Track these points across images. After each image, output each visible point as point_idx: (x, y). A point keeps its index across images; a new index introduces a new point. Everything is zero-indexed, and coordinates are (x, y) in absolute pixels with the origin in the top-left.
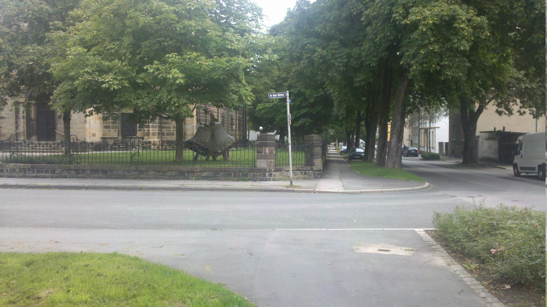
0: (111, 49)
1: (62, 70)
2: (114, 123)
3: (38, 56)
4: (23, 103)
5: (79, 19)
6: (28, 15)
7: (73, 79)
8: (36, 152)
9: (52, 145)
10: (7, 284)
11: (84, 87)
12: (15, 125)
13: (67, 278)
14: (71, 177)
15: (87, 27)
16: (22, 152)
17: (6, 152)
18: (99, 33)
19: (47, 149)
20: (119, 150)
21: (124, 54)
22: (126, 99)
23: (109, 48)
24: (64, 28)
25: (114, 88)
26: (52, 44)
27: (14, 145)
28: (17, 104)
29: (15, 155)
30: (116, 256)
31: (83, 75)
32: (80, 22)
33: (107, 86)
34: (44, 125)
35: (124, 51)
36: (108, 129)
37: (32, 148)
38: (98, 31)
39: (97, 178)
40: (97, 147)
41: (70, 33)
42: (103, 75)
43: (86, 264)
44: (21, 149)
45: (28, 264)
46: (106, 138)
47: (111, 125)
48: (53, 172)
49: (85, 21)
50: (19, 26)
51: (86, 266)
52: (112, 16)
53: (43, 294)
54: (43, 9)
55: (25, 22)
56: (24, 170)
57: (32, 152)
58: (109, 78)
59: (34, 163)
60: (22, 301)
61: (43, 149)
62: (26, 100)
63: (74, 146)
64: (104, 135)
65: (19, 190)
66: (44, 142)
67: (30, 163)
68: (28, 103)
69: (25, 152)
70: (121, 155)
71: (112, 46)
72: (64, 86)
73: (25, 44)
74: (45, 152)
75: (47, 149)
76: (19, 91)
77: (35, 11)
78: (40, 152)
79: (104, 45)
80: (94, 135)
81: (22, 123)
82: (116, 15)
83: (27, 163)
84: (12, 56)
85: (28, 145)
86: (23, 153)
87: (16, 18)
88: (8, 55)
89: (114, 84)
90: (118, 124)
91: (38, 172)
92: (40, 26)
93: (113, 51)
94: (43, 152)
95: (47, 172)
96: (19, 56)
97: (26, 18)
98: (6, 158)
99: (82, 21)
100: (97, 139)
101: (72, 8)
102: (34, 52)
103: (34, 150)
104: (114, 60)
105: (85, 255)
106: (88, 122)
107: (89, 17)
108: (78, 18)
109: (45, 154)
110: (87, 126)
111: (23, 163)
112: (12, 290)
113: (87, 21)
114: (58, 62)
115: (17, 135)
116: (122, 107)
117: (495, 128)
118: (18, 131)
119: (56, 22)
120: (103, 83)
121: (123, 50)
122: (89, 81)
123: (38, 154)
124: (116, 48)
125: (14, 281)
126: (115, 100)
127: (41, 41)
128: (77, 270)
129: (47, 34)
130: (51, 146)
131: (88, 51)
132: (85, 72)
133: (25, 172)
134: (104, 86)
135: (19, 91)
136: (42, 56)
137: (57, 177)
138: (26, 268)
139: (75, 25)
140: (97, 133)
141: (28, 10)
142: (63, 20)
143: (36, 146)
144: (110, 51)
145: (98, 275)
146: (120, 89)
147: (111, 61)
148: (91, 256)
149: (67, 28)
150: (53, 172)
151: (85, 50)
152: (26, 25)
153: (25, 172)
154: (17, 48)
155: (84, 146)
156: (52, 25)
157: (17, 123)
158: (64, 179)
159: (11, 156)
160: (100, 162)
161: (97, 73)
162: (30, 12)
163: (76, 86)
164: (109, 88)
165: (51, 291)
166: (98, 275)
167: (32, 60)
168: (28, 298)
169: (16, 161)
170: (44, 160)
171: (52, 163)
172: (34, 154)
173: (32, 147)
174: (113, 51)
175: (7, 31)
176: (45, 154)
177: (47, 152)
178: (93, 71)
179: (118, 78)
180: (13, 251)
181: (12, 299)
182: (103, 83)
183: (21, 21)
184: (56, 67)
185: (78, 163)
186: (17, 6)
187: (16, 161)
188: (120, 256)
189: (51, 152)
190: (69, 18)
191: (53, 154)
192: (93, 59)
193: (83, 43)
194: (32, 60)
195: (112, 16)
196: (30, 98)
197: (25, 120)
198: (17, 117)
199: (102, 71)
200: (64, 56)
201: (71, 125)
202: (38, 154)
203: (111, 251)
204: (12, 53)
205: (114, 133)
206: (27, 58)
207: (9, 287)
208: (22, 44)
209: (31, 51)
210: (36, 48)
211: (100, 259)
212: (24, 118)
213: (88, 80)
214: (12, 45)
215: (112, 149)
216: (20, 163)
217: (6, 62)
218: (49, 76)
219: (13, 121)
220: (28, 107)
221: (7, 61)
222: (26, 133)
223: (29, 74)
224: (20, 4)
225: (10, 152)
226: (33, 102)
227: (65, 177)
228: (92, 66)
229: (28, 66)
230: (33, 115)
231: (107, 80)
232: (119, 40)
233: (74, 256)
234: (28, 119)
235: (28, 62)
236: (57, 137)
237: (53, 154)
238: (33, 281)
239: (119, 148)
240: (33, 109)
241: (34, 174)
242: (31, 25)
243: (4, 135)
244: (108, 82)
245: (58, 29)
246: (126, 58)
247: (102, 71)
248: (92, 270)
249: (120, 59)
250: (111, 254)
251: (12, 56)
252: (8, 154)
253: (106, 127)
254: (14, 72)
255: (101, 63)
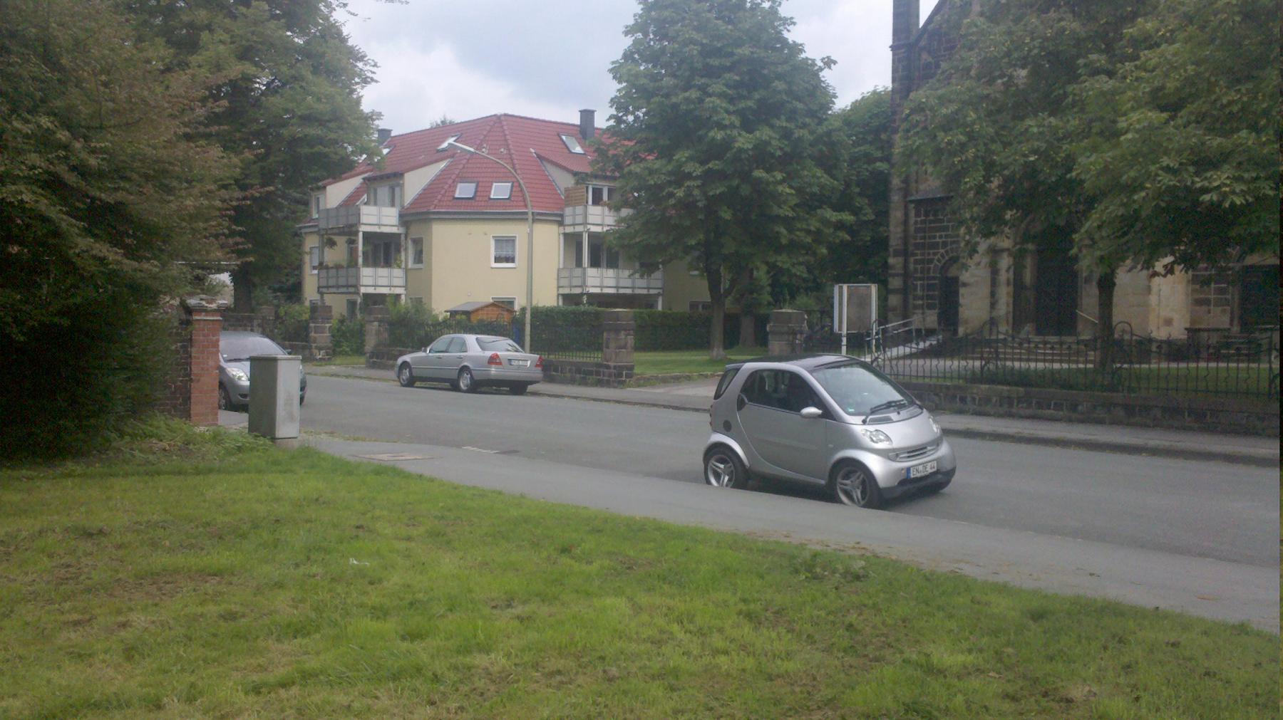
0: (1230, 103)
1: (1106, 169)
2: (1221, 291)
3: (1047, 141)
4: (1008, 250)
5: (1149, 42)
6: (1030, 51)
7: (1133, 188)
8: (1037, 361)
9: (1074, 347)
10: (996, 653)
11: (1157, 205)
12: (987, 302)
13: (1129, 667)
14: (1115, 422)
15: (1173, 58)
16: (1006, 359)
17: (973, 359)
18: (1202, 69)
19: (1053, 354)
20: (1238, 361)
21: (1266, 113)
22: (1265, 227)
23: (1225, 101)
24: (1110, 67)
25: (1233, 204)
26: (1082, 110)
27: (988, 343)
28: (995, 252)
29: (991, 366)
30: (1247, 634)
31: (1157, 175)
32: (1150, 47)
33: (1215, 198)
34: (1051, 299)
35: (1265, 105)
36: (1205, 308)
37: (1029, 351)
38: (1197, 63)
39: (1177, 428)
40: (1174, 351)
41: (1125, 78)
42: (1207, 170)
43: (1172, 640)
44: (1005, 353)
45: (1038, 616)
46: (1199, 330)
47: (1212, 297)
48: (1074, 407)
49: (1164, 46)
50: (1011, 77)
51: (1173, 645)
52: (1238, 19)
53: (1077, 692)
54: (1065, 30)
55: (1023, 67)
56: (1010, 401)
57: (1028, 360)
58: (1220, 177)
59: (1031, 385)
60: (1032, 699)
61: (1045, 354)
62: (1016, 244)
63: (1117, 347)
64: (1193, 322)
65: (997, 445)
66: (1053, 339)
67: (1024, 385)
68: (1020, 250)
69: (1013, 360)
70: (1243, 375)
71: (1228, 96)
72: (1107, 208)
73: (1022, 118)
74: (1057, 361)
75: (1053, 354)
76: (1001, 221)
77: (1046, 39)
78: (1044, 361)
79: (1213, 97)
80: (1169, 322)
81: (1005, 295)
82: (1247, 16)
83: (1016, 385)
84: (993, 147)
85: (1021, 344)
86: (1009, 363)
87: (1006, 60)
88: (985, 144)
89: (1233, 192)
90: (1234, 294)
91: (1040, 405)
92: (1056, 70)
93: (1235, 109)
94: (1052, 361)
95: (1058, 407)
96: (1006, 145)
97: (1025, 58)
98: (973, 372)
99: (1158, 45)
100: (1178, 331)
101: (1133, 17)
102: (1040, 133)
103: (1031, 356)
104: (1238, 130)
105: (1166, 616)
106: (1155, 289)
107: (1172, 31)
108: (1145, 40)
109: (1056, 366)
110: (1153, 299)
111: (1009, 384)
112: (1008, 668)
113: (1171, 41)
114: (1095, 149)
115: (993, 322)
116: (1252, 250)
117: (965, 285)
118: (994, 314)
119: (1093, 57)
120: (1205, 191)
121: (1263, 101)
122: (1171, 190)
123: (1041, 365)
124: (1245, 99)
125: (1010, 650)
126: (1233, 234)
127: (1055, 106)
128: (1151, 651)
129: (1070, 88)
130: (1069, 348)
131: (1172, 118)
132: (1162, 169)
133: (1011, 405)
134: (1206, 197)
135: (1001, 221)
136: (1059, 140)
137: (1082, 421)
138: (1031, 622)
139: (1138, 58)
140: (1176, 317)
141: (1033, 39)
142: (1109, 50)
143: (1036, 347)
144: (1227, 111)
145: (1207, 674)
146: (1248, 204)
147: (1226, 134)
148: (1185, 623)
149: (1119, 65)
150: (1074, 407)
151: (1165, 115)
152: (1023, 73)
153: (1011, 405)
154: (1003, 128)
155: (1144, 347)
156: (1085, 65)
157: (993, 294)
158: (1100, 428)
159: (982, 368)
160: (1158, 389)
161: (1191, 169)
162: (1036, 43)
163: (1136, 206)
164: (1220, 203)
165: (1095, 689)
166: (1207, 674)
167: (1035, 152)
168: (1045, 695)
169: (992, 379)
170: (1052, 379)
171: (1071, 387)
172: (1033, 365)
173: (1029, 350)
174: (1235, 109)
175: (985, 92)
176: (1056, 366)
177: (1061, 361)
178: (1181, 164)
179: (1246, 175)
180: (1000, 579)
181: (1010, 689)
182: (1205, 191)
183: (1015, 65)
184: (1090, 164)
185: (1130, 390)
186: (1010, 33)
187: (992, 379)
188: (1259, 635)
189: (1069, 362)
190: (1124, 42)
191: (1074, 366)
192: (1184, 134)
193: (1159, 101)
194: (1035, 152)
195: (1238, 19)
196: (1026, 237)
197: (1011, 289)
198: (994, 283)
199: (1204, 163)
200: (1112, 134)
201: (1115, 300)
202: (1041, 365)
203: (1234, 617)
204: (993, 141)
205: (1220, 318)
206: (1025, 148)
207: (1000, 660)
208: (1014, 118)
209: (1035, 130)
210: (1046, 123)
211: (1206, 633)
212: (1008, 284)
213: (1169, 187)
214: (996, 122)
215: (1218, 358)
216: (999, 383)
217: (980, 162)
218: (1071, 186)
219: (985, 290)
220: (1018, 257)
221: (983, 158)
222: (1011, 316)
223: (1026, 185)
224: (1014, 29)
225: (981, 359)
226: (1031, 247)
227: (1100, 422)
228: (1179, 152)
229: (1026, 164)
230: (1028, 276)
231: (1216, 184)
232: (1249, 78)
233: (1138, 614)
234: (1018, 285)
235: (1025, 156)
236: (1080, 327)
237: (1074, 366)
238: (1051, 659)
239: (1239, 355)
240: (1029, 262)
241: (1029, 412)
242: (1035, 73)
243: (966, 322)
244: (1218, 187)
245: (1096, 72)
246: (1269, 121)
247: (1204, 163)
248: (1190, 659)
249: (1254, 128)
250: (1233, 627)
251: (993, 147)
252: (977, 363)
253: (1199, 302)
254: (996, 182)
255: (1203, 144)
